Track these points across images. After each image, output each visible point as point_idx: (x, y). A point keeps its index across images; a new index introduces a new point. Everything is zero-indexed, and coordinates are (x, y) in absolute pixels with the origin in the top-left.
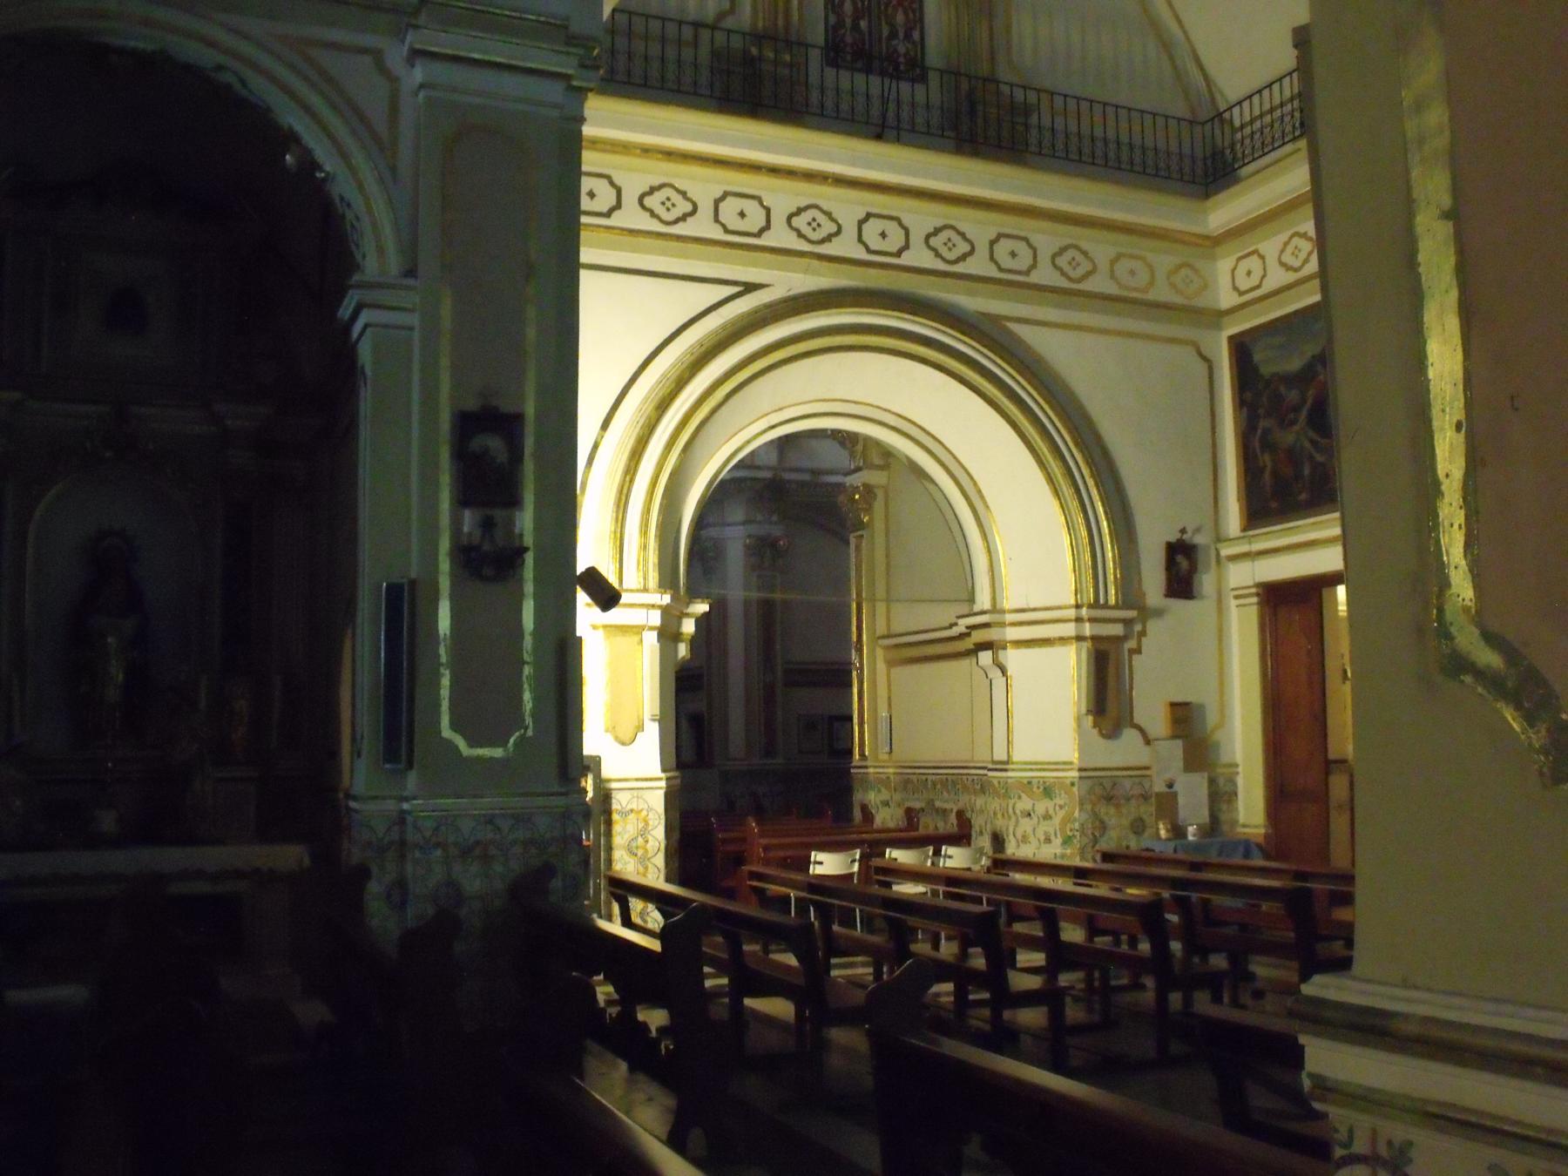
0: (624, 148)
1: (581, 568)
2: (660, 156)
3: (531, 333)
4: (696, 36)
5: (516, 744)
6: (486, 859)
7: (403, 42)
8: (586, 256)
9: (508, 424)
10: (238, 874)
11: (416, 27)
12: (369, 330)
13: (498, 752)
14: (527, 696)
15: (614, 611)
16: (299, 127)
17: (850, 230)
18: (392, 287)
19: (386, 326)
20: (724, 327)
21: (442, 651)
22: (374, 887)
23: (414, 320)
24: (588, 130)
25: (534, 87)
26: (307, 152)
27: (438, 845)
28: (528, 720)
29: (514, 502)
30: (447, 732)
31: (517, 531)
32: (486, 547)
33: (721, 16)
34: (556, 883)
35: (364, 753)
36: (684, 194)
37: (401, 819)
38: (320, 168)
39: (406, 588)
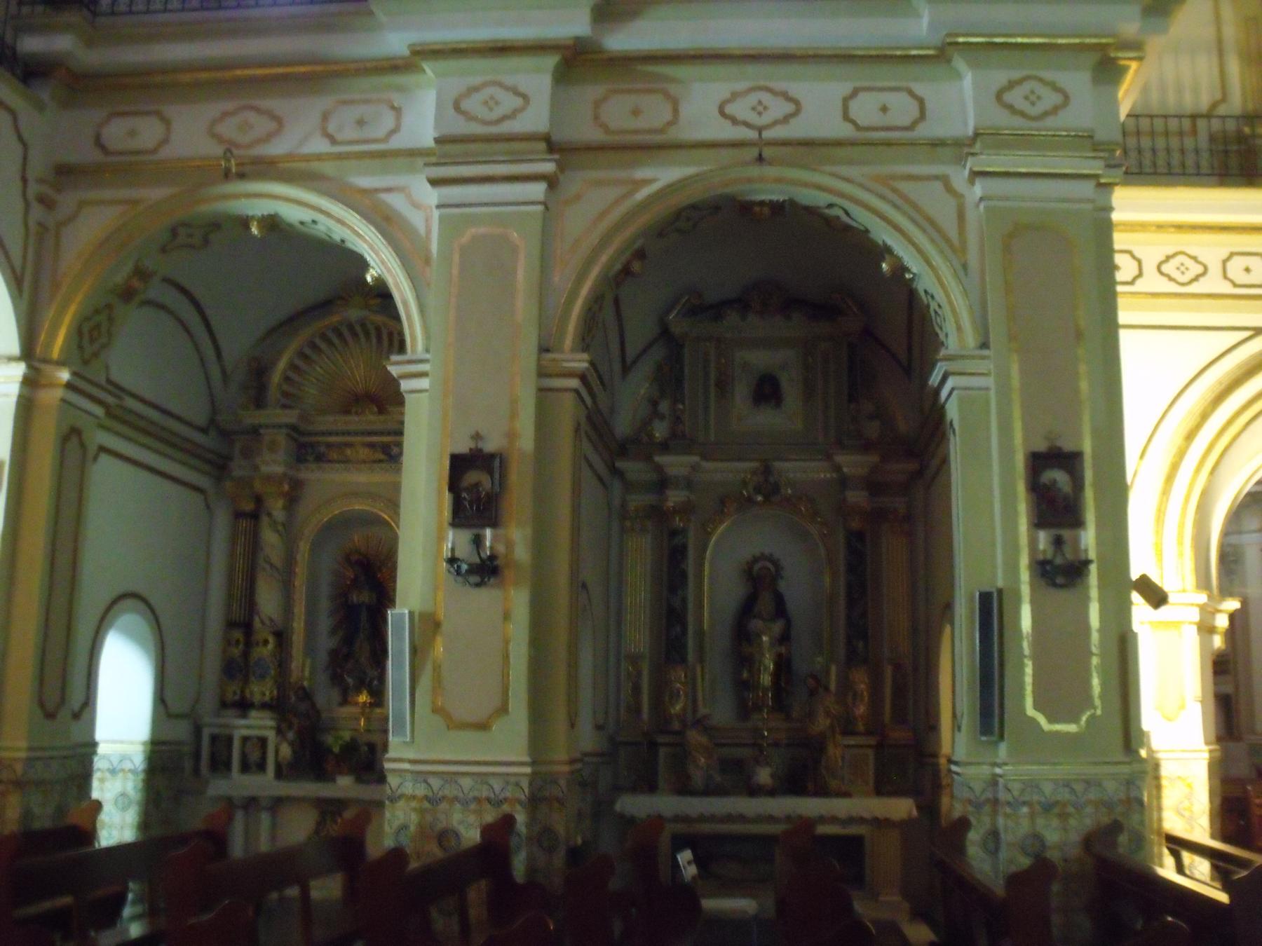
0: (1142, 227)
1: (1135, 575)
2: (1173, 230)
3: (1084, 385)
4: (1194, 126)
5: (1088, 721)
6: (1063, 816)
7: (964, 166)
8: (1123, 317)
9: (1068, 460)
10: (861, 820)
11: (973, 154)
12: (955, 393)
13: (1072, 728)
14: (1096, 682)
15: (1163, 609)
16: (889, 242)
17: (1215, 269)
18: (973, 357)
19: (966, 389)
20: (1239, 367)
21: (1025, 645)
22: (973, 836)
23: (990, 382)
24: (1115, 216)
25: (1065, 187)
26: (899, 259)
27: (1024, 803)
28: (1097, 702)
29: (1078, 523)
30: (1030, 711)
31: (1083, 547)
32: (1059, 561)
33: (1214, 105)
34: (1123, 839)
35: (964, 728)
36: (1195, 259)
37: (994, 781)
38: (907, 270)
39: (995, 595)
